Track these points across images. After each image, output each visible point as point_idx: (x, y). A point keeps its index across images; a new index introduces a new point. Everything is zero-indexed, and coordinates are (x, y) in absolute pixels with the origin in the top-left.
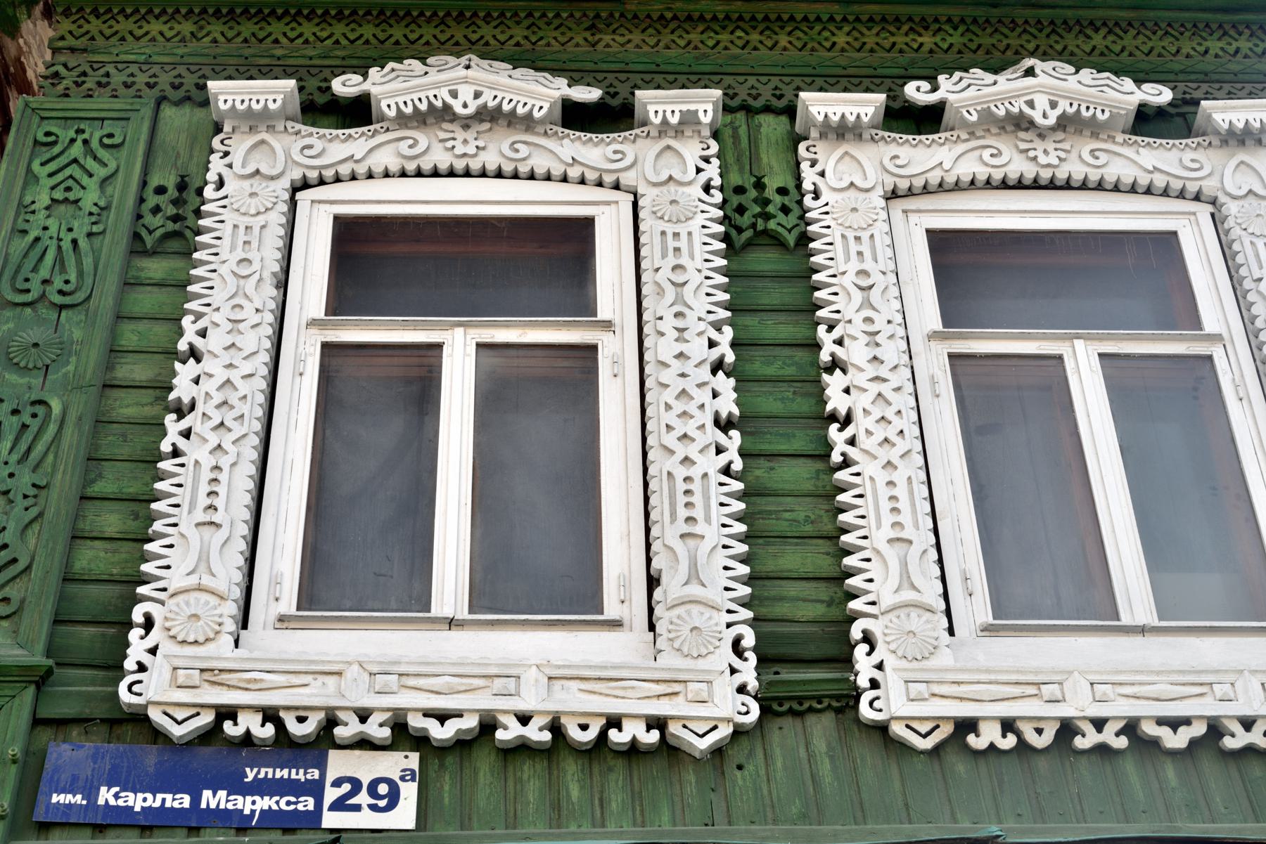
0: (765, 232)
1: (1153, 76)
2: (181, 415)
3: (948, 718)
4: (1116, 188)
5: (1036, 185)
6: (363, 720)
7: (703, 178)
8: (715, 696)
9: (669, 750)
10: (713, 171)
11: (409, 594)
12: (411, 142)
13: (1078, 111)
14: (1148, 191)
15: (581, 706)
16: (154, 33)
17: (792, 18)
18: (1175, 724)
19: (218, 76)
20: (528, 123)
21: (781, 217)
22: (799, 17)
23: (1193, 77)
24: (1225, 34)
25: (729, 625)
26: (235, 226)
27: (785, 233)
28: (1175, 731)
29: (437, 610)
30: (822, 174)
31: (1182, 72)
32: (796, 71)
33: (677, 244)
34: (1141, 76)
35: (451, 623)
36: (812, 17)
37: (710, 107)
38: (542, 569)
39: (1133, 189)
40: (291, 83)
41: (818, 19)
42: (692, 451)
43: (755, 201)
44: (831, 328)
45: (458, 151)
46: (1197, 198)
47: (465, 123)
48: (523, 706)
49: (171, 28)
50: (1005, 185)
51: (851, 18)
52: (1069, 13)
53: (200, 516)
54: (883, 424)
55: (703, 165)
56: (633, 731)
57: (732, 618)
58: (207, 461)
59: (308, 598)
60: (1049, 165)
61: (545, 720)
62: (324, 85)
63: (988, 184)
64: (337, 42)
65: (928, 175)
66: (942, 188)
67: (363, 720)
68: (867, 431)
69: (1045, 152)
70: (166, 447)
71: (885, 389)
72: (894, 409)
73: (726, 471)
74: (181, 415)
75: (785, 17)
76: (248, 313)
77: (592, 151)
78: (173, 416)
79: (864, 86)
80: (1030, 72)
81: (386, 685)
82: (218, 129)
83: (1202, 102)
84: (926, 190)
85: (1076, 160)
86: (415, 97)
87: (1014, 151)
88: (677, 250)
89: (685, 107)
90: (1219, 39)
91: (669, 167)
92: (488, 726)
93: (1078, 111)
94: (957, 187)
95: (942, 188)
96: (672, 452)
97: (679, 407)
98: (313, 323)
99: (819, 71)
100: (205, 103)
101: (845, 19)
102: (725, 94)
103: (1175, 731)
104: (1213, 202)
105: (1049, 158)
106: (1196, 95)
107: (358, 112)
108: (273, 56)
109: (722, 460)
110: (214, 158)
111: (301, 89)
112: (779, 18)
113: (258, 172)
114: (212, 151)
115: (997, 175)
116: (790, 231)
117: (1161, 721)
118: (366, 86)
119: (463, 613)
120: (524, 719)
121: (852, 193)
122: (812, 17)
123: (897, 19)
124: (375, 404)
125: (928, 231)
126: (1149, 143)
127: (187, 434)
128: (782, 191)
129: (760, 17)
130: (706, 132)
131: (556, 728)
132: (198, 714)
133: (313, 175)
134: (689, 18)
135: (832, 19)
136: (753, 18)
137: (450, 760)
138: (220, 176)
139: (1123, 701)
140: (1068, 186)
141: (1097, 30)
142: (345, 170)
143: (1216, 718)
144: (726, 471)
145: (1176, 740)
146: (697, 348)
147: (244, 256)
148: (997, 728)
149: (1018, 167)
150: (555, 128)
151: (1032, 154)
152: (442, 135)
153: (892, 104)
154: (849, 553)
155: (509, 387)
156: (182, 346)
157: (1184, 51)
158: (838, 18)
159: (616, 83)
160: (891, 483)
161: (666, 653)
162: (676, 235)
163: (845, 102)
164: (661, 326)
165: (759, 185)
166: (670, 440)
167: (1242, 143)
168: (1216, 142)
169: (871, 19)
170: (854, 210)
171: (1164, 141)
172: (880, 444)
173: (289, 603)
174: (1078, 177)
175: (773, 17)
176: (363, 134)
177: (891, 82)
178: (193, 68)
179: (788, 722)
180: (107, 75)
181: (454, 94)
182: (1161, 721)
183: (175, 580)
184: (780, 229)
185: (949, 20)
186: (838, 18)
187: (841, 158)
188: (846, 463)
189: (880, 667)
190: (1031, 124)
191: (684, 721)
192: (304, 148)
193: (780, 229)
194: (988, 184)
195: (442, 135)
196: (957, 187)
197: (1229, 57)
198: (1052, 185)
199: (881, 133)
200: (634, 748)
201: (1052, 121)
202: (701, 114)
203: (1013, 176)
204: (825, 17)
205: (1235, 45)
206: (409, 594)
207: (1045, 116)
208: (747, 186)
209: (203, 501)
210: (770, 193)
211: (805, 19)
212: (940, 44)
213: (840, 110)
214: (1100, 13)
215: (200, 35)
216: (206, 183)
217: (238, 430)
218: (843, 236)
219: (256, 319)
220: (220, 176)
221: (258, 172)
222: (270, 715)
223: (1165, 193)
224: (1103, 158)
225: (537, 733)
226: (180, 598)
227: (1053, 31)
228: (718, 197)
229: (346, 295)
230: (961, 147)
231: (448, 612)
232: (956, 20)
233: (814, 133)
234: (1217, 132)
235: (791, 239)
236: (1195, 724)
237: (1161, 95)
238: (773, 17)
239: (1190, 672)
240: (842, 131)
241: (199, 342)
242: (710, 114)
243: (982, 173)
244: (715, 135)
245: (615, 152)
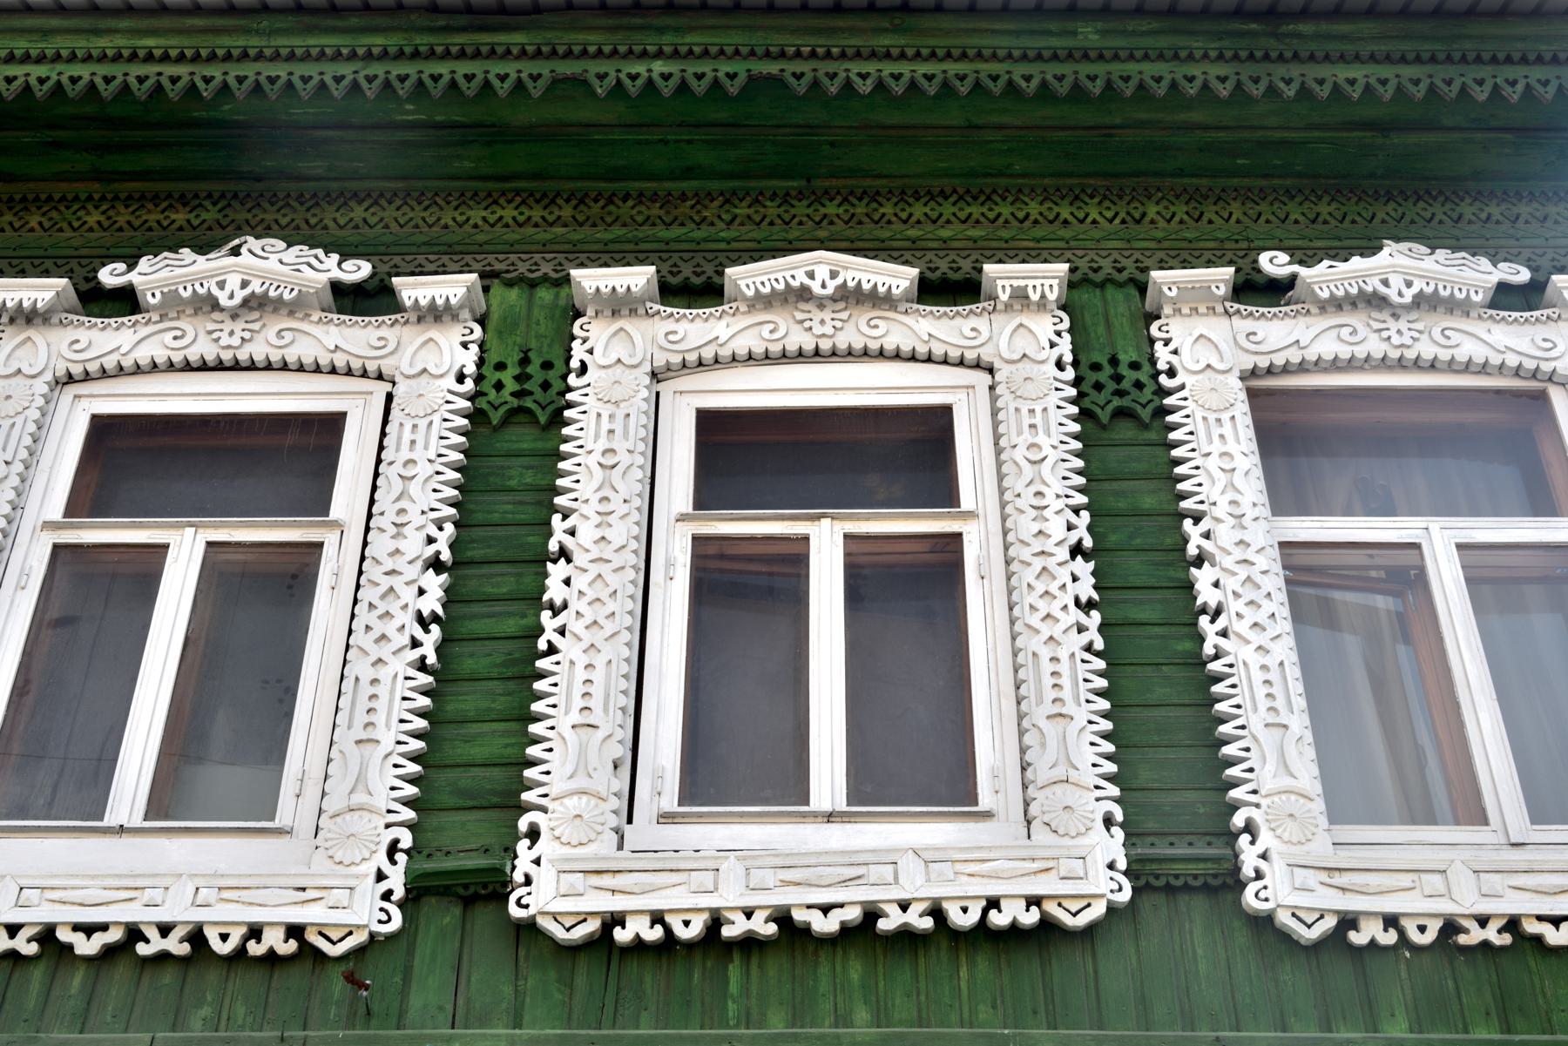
0: (521, 410)
1: (827, 244)
2: (556, 612)
3: (641, 912)
4: (301, 368)
5: (220, 367)
6: (749, 915)
7: (1056, 352)
8: (1087, 871)
9: (308, 953)
10: (1065, 348)
11: (786, 784)
12: (771, 326)
13: (787, 283)
14: (333, 371)
15: (224, 920)
16: (975, 216)
17: (50, 198)
18: (88, 930)
19: (990, 259)
20: (295, 307)
21: (1135, 393)
22: (57, 196)
23: (436, 249)
24: (1447, 199)
25: (388, 826)
26: (599, 415)
27: (1138, 408)
28: (89, 937)
29: (110, 820)
30: (591, 352)
31: (425, 244)
32: (28, 253)
33: (1033, 421)
34: (347, 250)
35: (830, 817)
36: (70, 197)
37: (1055, 282)
38: (916, 758)
39: (317, 369)
40: (653, 269)
41: (76, 198)
42: (1057, 631)
43: (1111, 377)
44: (565, 517)
45: (223, 343)
46: (977, 365)
47: (821, 303)
48: (165, 916)
49: (197, 216)
50: (187, 367)
51: (109, 196)
52: (335, 185)
53: (575, 717)
54: (1047, 598)
55: (1056, 339)
56: (273, 939)
57: (392, 818)
58: (581, 661)
59: (688, 794)
60: (229, 347)
61: (923, 906)
62: (91, 275)
63: (171, 367)
64: (387, 227)
65: (103, 360)
66: (121, 371)
67: (749, 915)
68: (1031, 606)
69: (822, 322)
70: (542, 645)
71: (605, 569)
72: (1058, 583)
73: (1089, 648)
74: (556, 612)
75: (43, 197)
76: (616, 504)
77: (356, 337)
78: (549, 613)
79: (1226, 258)
80: (235, 252)
81: (572, 885)
82: (578, 314)
83: (727, 271)
84: (104, 374)
85: (857, 330)
86: (758, 280)
87: (791, 321)
88: (1033, 426)
89: (1016, 283)
90: (954, 204)
91: (1023, 344)
92: (872, 914)
93: (787, 283)
94: (138, 370)
95: (121, 371)
96: (1037, 632)
97: (1040, 587)
98: (682, 518)
99: (51, 252)
100: (1142, 289)
101: (103, 198)
102: (482, 276)
103: (89, 937)
104: (991, 371)
105: (224, 339)
106: (1147, 262)
107: (125, 302)
108: (1001, 239)
109: (1084, 638)
110: (576, 344)
111: (658, 271)
112: (37, 199)
113: (19, 371)
114: (573, 338)
115: (775, 348)
116: (1144, 406)
117: (77, 928)
118: (134, 277)
119: (842, 805)
120: (904, 906)
121: (619, 369)
122: (70, 197)
123: (156, 196)
124: (743, 595)
125: (344, 414)
126: (945, 314)
127: (562, 631)
128: (1135, 366)
129: (18, 197)
130: (1054, 306)
131: (937, 912)
132: (1089, 905)
133: (77, 370)
134: (143, 197)
135: (90, 198)
136: (37, 199)
137: (698, 956)
138: (583, 362)
139: (47, 906)
140: (252, 367)
141: (1292, 198)
142: (708, 354)
143: (135, 924)
144: (1089, 648)
145: (87, 946)
146: (1056, 528)
147: (607, 446)
148: (647, 920)
149: (799, 339)
150: (330, 316)
151: (807, 324)
152: (211, 326)
153: (929, 274)
154: (1224, 722)
155: (867, 575)
156: (553, 546)
157: (1293, 217)
158: (96, 196)
159: (680, 263)
160: (1054, 659)
161: (1039, 832)
162: (1032, 411)
163: (28, 287)
164: (1020, 503)
165: (1114, 361)
166: (1035, 620)
167: (1340, 307)
168: (743, 308)
169: (130, 197)
170: (9, 397)
171: (359, 319)
172: (1043, 620)
173: (670, 802)
174: (858, 345)
175: (30, 197)
176: (1251, 314)
177: (1240, 252)
178: (60, 262)
179: (1160, 899)
180: (675, 265)
181: (811, 275)
182: (77, 928)
183: (556, 785)
184: (1134, 405)
185: (210, 196)
186: (96, 196)
187: (615, 334)
188: (552, 650)
189: (537, 862)
190: (215, 305)
191: (1059, 899)
192: (182, 337)
193: (1134, 405)
194: (171, 367)
195: (211, 326)
196: (138, 370)
197: (693, 226)
198: (236, 366)
199: (915, 306)
200: (639, 944)
201: (830, 291)
202: (1030, 290)
203: (792, 347)
204: (83, 196)
205: (968, 210)
206: (786, 784)
207: (824, 286)
208: (509, 362)
209: (578, 702)
210: (1124, 370)
211: (63, 199)
212: (1046, 213)
213: (17, 296)
214: (367, 184)
215: (253, 223)
216: (569, 371)
217: (609, 627)
218: (1017, 410)
219: (625, 508)
220: (583, 362)
221: (19, 371)
222: (657, 918)
223: (349, 372)
224: (288, 336)
225: (175, 945)
226: (1047, 791)
227: (698, 202)
228: (1070, 374)
229: (713, 487)
230: (144, 331)
231: (826, 806)
232: (216, 195)
233: (1167, 310)
234: (745, 299)
235: (1145, 414)
236: (112, 929)
237: (358, 271)
238: (30, 197)
239: (127, 876)
240: (619, 305)
241: (569, 541)
242: (1056, 289)
243: (161, 357)
244: (1063, 308)
245: (380, 339)
